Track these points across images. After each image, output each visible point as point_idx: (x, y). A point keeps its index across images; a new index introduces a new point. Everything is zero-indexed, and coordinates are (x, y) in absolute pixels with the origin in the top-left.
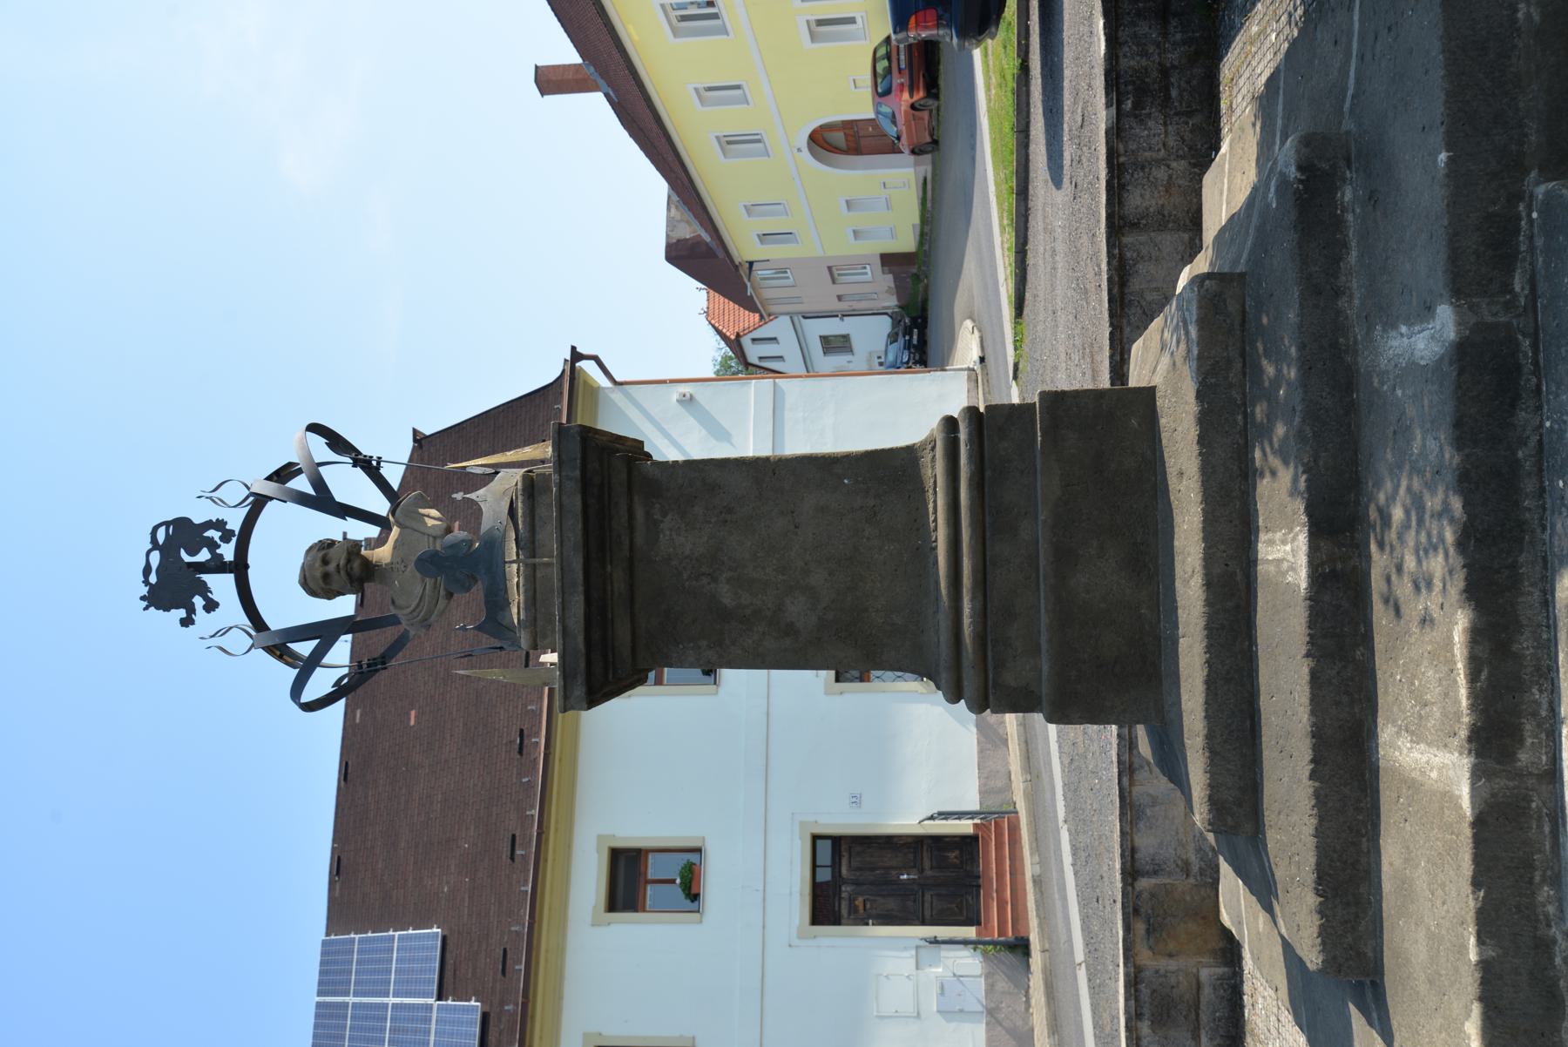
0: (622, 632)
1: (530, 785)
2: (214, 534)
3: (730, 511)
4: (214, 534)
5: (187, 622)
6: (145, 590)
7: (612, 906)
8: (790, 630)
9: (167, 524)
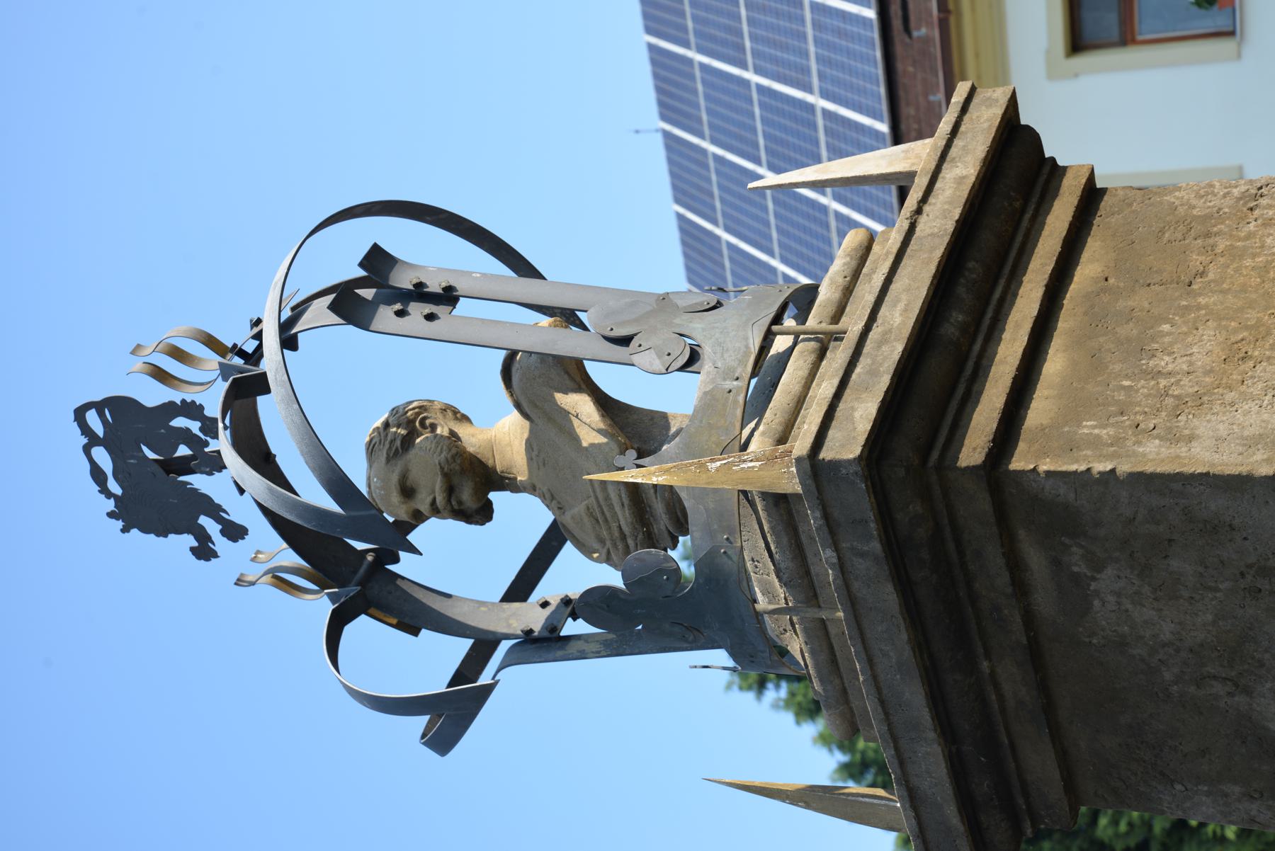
0: (1040, 764)
2: (195, 426)
4: (195, 426)
5: (204, 551)
6: (110, 505)
7: (1077, 43)
9: (99, 406)
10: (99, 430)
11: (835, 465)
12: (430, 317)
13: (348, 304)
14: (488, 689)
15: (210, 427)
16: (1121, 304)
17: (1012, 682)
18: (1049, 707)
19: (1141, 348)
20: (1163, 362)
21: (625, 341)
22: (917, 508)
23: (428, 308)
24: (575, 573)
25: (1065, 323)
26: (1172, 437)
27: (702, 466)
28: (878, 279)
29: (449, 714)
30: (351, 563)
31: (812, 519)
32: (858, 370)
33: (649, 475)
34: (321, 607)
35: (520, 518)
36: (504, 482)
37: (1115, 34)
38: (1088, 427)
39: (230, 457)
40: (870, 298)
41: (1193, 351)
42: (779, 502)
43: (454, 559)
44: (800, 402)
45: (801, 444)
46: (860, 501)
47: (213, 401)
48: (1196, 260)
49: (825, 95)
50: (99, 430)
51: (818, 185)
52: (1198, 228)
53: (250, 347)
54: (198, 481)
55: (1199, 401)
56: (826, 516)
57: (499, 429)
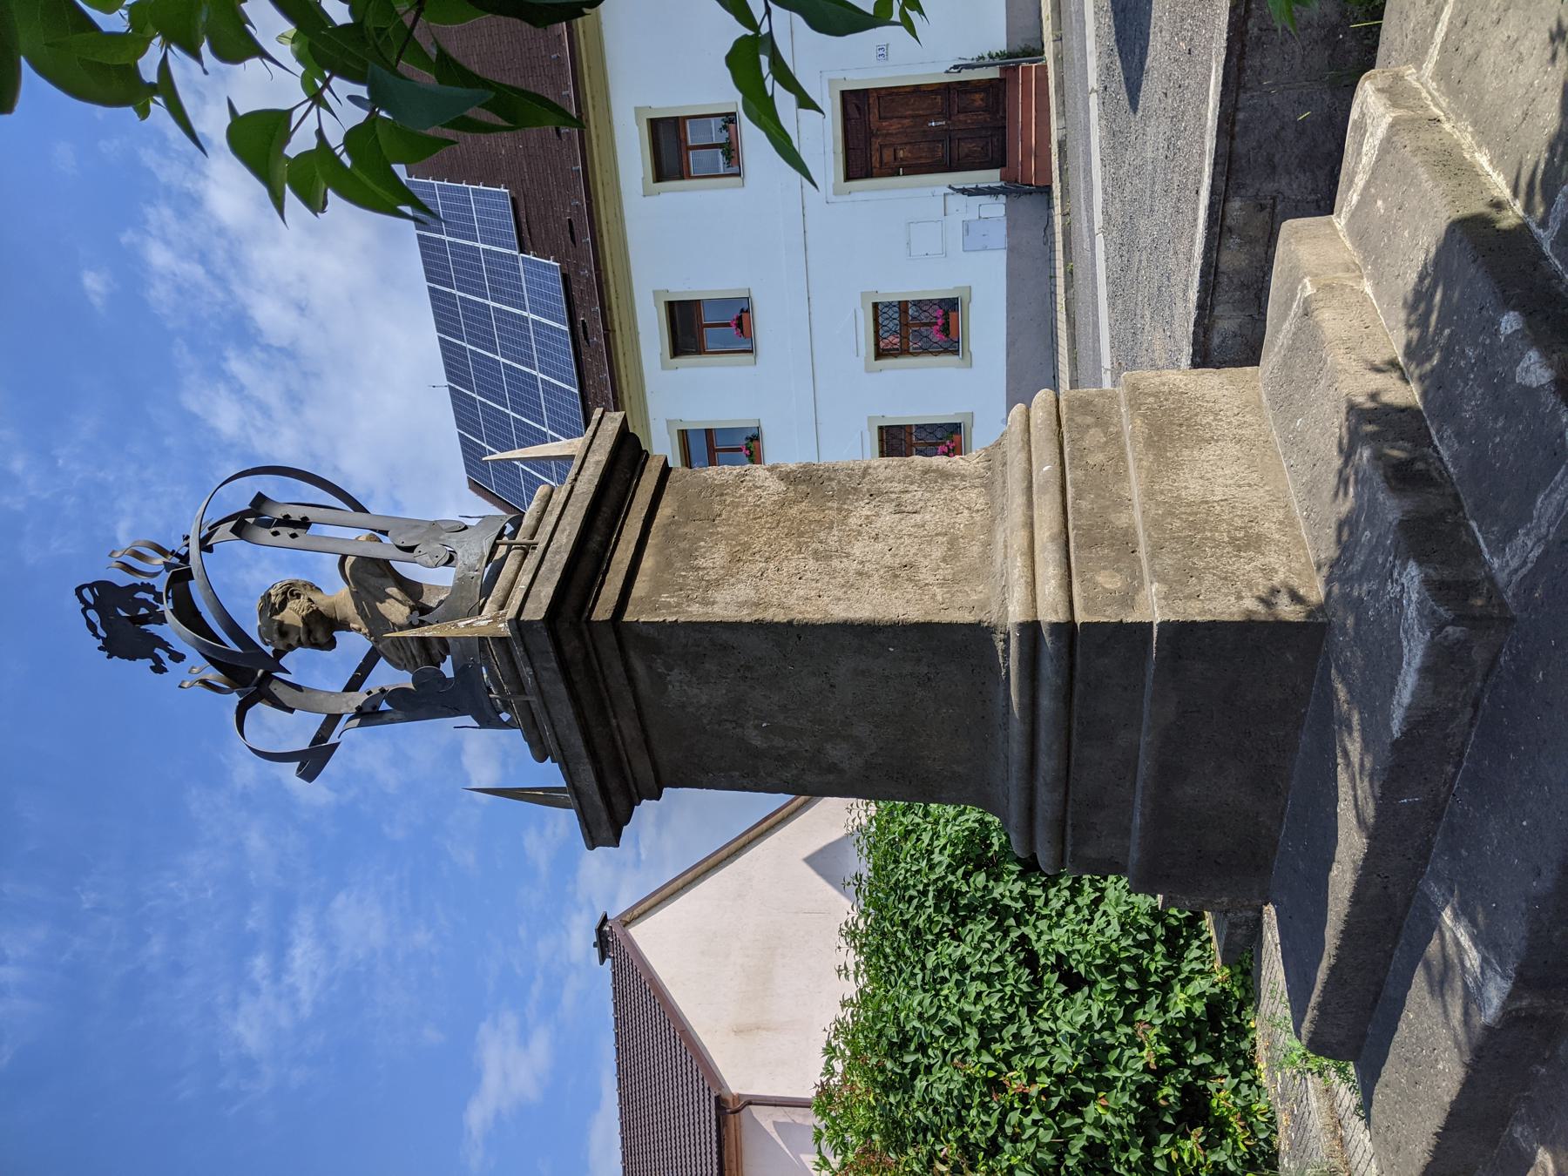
1: (559, 62)
2: (150, 597)
3: (749, 668)
4: (150, 597)
6: (100, 643)
7: (660, 176)
8: (833, 768)
9: (91, 586)
10: (91, 600)
11: (531, 623)
12: (294, 536)
13: (241, 526)
14: (335, 746)
15: (158, 597)
16: (681, 531)
17: (628, 728)
18: (647, 741)
19: (690, 555)
20: (701, 562)
21: (411, 549)
22: (576, 643)
23: (292, 531)
24: (387, 676)
25: (651, 541)
26: (706, 602)
27: (456, 626)
28: (553, 519)
29: (313, 760)
30: (250, 675)
31: (518, 652)
32: (543, 568)
33: (427, 632)
34: (235, 698)
35: (353, 644)
36: (344, 625)
37: (661, 129)
38: (664, 598)
39: (169, 616)
40: (550, 529)
41: (714, 558)
42: (501, 641)
43: (318, 672)
44: (513, 583)
45: (511, 612)
46: (544, 642)
47: (161, 584)
48: (717, 508)
49: (542, 371)
50: (91, 600)
51: (521, 460)
52: (718, 491)
53: (183, 553)
54: (153, 628)
55: (718, 583)
56: (526, 650)
57: (337, 594)
